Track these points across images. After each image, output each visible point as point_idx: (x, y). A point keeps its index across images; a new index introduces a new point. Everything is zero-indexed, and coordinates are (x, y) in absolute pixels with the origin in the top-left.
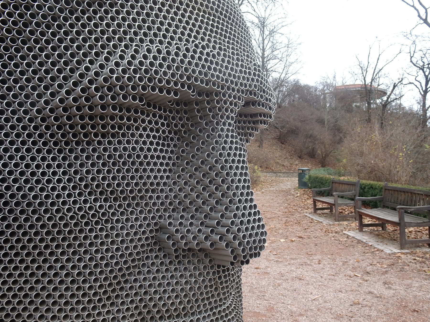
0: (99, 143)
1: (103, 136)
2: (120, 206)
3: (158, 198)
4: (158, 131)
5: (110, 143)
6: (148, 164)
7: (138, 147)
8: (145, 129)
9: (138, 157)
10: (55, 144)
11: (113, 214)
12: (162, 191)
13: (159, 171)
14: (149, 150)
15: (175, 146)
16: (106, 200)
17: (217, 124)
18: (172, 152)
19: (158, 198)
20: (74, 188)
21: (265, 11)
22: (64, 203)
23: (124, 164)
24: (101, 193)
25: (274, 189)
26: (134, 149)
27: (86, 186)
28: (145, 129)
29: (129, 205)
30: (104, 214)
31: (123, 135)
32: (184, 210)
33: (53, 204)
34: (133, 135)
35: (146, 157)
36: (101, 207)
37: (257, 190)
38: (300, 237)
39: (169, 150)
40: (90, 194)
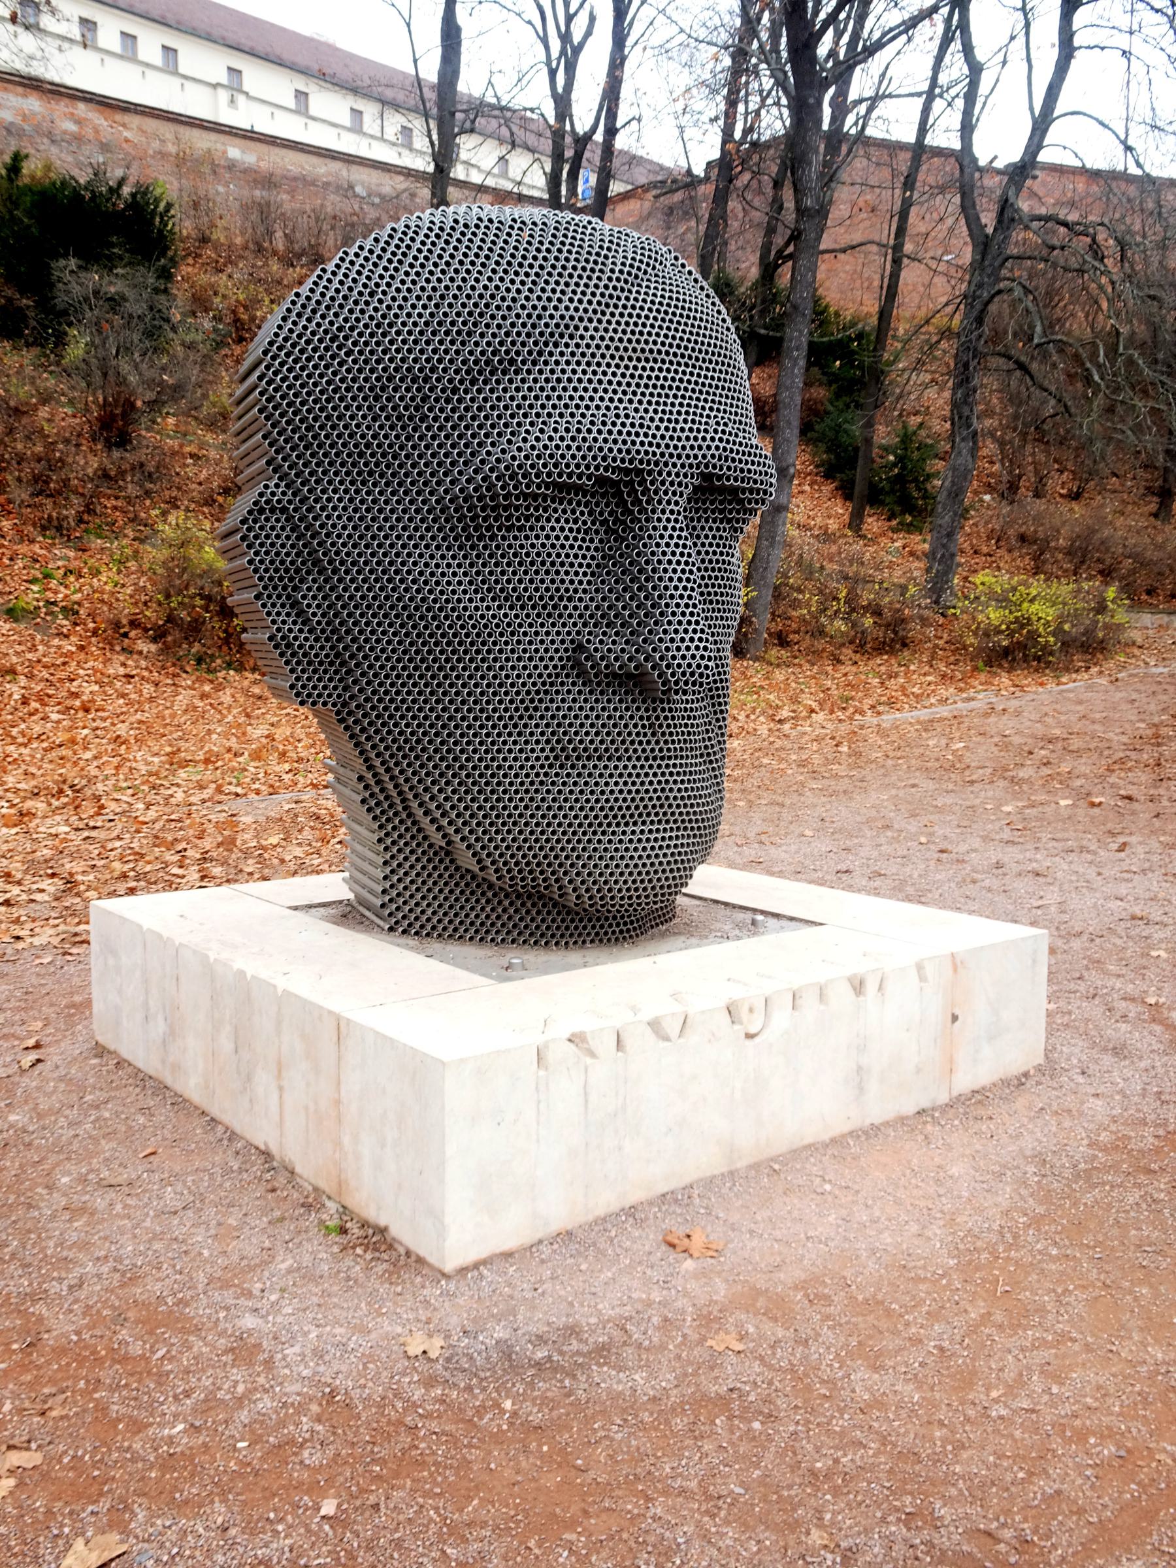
0: (504, 538)
1: (509, 529)
2: (528, 616)
3: (576, 608)
4: (576, 521)
5: (515, 538)
6: (562, 564)
7: (548, 543)
8: (558, 520)
9: (549, 555)
10: (455, 539)
11: (520, 625)
12: (580, 600)
13: (577, 574)
14: (563, 546)
15: (601, 541)
16: (511, 608)
17: (653, 512)
18: (596, 549)
19: (576, 608)
20: (476, 591)
21: (1103, 48)
22: (465, 609)
23: (532, 563)
24: (506, 599)
25: (1166, 670)
26: (543, 545)
27: (489, 590)
28: (558, 520)
29: (538, 615)
30: (509, 625)
31: (532, 529)
32: (608, 626)
33: (453, 609)
34: (543, 529)
35: (559, 555)
36: (506, 616)
37: (1101, 672)
38: (1130, 798)
39: (593, 546)
40: (493, 599)
